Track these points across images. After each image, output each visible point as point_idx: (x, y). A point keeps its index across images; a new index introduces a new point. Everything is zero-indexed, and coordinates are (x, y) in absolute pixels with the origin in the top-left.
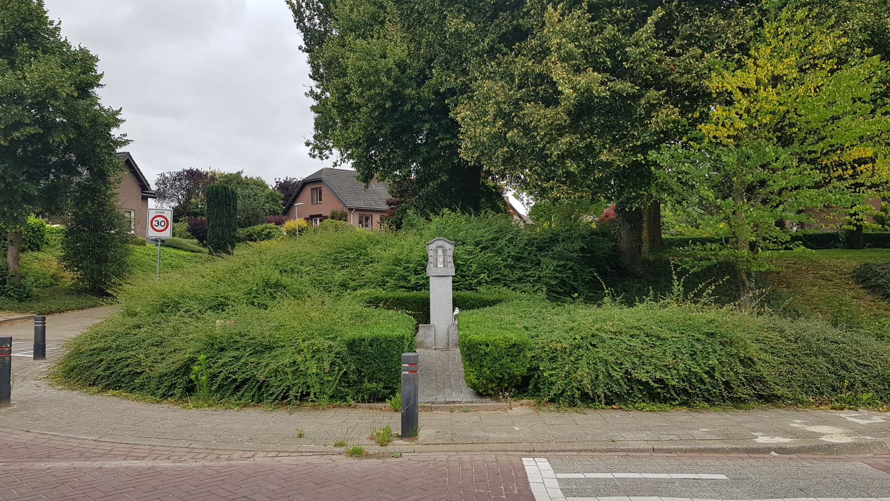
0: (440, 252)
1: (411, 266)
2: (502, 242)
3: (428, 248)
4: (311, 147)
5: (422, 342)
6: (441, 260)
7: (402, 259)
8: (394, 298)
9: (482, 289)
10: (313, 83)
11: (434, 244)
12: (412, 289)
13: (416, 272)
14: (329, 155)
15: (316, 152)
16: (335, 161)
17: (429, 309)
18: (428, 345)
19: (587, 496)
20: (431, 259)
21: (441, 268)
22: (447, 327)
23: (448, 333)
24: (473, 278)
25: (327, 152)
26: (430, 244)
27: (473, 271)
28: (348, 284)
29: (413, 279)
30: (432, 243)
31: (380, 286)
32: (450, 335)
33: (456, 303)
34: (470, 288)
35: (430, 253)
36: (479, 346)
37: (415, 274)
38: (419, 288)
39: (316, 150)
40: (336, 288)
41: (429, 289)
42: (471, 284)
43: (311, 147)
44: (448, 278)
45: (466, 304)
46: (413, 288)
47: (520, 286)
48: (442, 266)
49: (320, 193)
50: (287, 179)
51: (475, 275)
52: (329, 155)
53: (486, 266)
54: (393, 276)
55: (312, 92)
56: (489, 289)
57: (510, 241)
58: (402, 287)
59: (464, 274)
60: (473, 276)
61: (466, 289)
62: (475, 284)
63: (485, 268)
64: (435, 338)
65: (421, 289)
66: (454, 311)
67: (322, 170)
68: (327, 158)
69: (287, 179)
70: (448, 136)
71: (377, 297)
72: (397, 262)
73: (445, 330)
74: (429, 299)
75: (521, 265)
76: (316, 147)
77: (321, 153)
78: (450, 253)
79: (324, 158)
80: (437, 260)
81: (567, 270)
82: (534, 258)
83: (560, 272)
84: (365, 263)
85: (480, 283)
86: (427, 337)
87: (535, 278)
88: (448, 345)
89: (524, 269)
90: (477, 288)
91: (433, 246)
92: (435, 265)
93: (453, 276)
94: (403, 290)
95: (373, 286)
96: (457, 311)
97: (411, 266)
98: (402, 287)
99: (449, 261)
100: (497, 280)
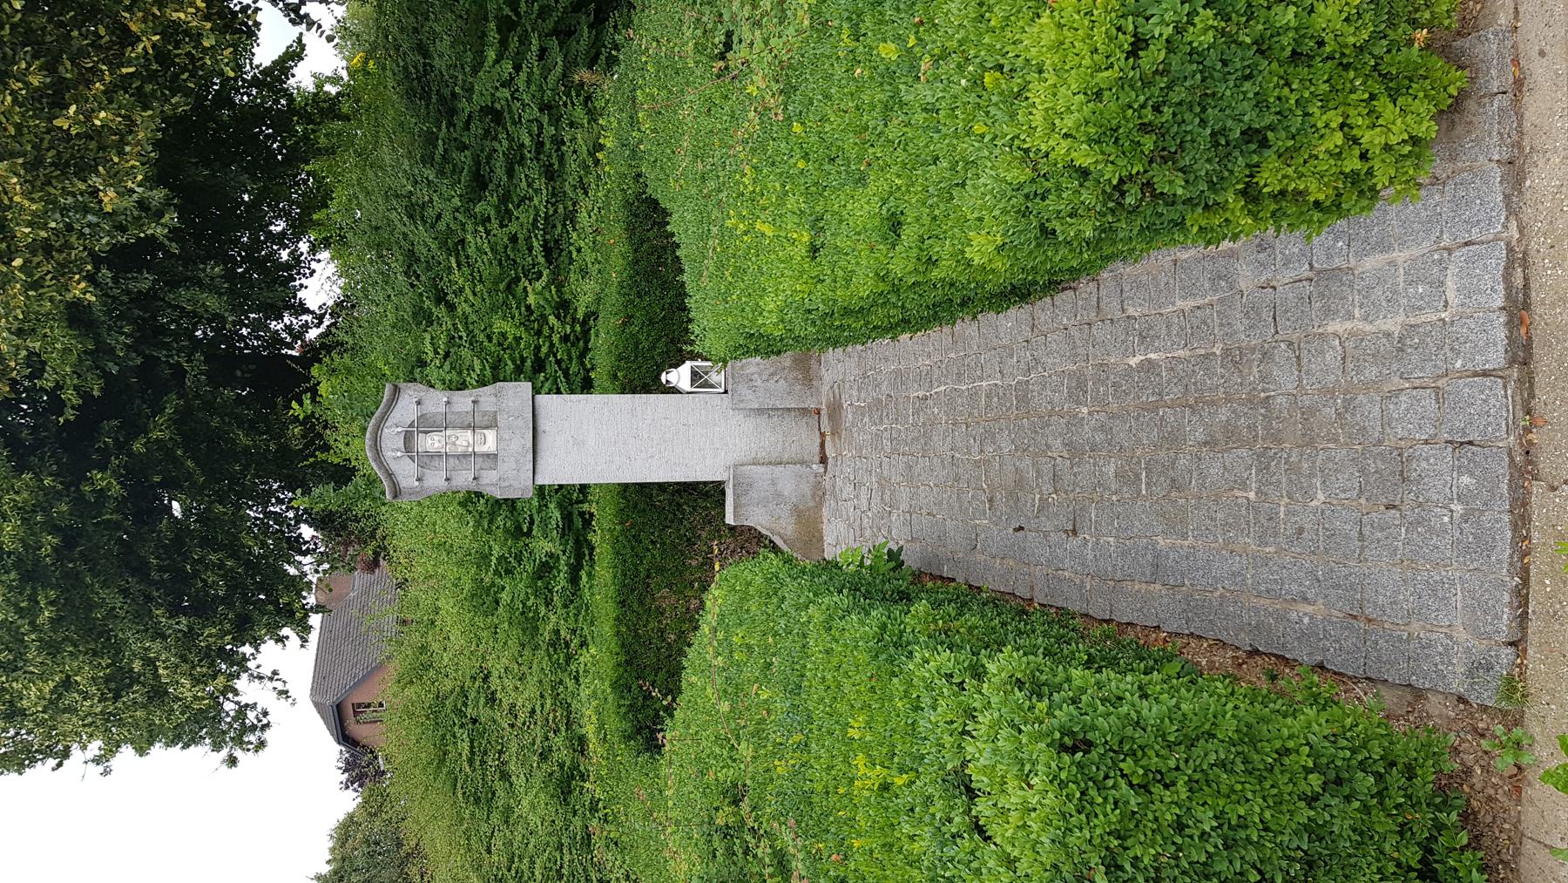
0: (432, 442)
1: (497, 551)
2: (423, 239)
3: (413, 492)
4: (238, 753)
5: (799, 513)
6: (464, 440)
7: (474, 580)
8: (617, 619)
9: (584, 294)
10: (77, 754)
11: (394, 467)
12: (581, 552)
13: (519, 533)
14: (259, 710)
15: (252, 738)
16: (275, 694)
17: (662, 487)
18: (806, 489)
20: (464, 480)
21: (499, 439)
23: (760, 411)
24: (546, 331)
25: (251, 715)
27: (521, 332)
28: (561, 766)
29: (544, 546)
30: (390, 475)
31: (569, 658)
32: (770, 403)
33: (649, 383)
34: (581, 339)
35: (436, 481)
36: (1153, 56)
37: (529, 534)
38: (578, 523)
39: (246, 739)
40: (577, 822)
41: (584, 488)
42: (565, 339)
43: (238, 753)
44: (541, 412)
45: (646, 344)
46: (577, 542)
47: (572, 165)
48: (491, 435)
49: (359, 705)
50: (340, 768)
51: (533, 321)
53: (502, 286)
54: (536, 612)
55: (97, 761)
56: (584, 273)
57: (415, 211)
58: (574, 579)
59: (528, 363)
60: (539, 333)
61: (582, 355)
62: (564, 323)
63: (508, 287)
64: (770, 463)
65: (582, 514)
66: (674, 391)
67: (316, 704)
68: (265, 714)
69: (340, 768)
71: (614, 686)
72: (484, 599)
73: (749, 424)
74: (625, 487)
75: (500, 172)
76: (239, 741)
77: (253, 728)
78: (436, 400)
79: (265, 721)
80: (465, 456)
81: (518, 14)
82: (476, 128)
83: (524, 41)
84: (492, 700)
85: (563, 307)
86: (779, 495)
87: (545, 120)
88: (804, 412)
89: (515, 160)
90: (580, 315)
91: (406, 473)
92: (489, 463)
93: (536, 391)
94: (585, 578)
95: (570, 683)
96: (680, 376)
97: (497, 551)
98: (574, 579)
99: (470, 407)
100: (551, 250)
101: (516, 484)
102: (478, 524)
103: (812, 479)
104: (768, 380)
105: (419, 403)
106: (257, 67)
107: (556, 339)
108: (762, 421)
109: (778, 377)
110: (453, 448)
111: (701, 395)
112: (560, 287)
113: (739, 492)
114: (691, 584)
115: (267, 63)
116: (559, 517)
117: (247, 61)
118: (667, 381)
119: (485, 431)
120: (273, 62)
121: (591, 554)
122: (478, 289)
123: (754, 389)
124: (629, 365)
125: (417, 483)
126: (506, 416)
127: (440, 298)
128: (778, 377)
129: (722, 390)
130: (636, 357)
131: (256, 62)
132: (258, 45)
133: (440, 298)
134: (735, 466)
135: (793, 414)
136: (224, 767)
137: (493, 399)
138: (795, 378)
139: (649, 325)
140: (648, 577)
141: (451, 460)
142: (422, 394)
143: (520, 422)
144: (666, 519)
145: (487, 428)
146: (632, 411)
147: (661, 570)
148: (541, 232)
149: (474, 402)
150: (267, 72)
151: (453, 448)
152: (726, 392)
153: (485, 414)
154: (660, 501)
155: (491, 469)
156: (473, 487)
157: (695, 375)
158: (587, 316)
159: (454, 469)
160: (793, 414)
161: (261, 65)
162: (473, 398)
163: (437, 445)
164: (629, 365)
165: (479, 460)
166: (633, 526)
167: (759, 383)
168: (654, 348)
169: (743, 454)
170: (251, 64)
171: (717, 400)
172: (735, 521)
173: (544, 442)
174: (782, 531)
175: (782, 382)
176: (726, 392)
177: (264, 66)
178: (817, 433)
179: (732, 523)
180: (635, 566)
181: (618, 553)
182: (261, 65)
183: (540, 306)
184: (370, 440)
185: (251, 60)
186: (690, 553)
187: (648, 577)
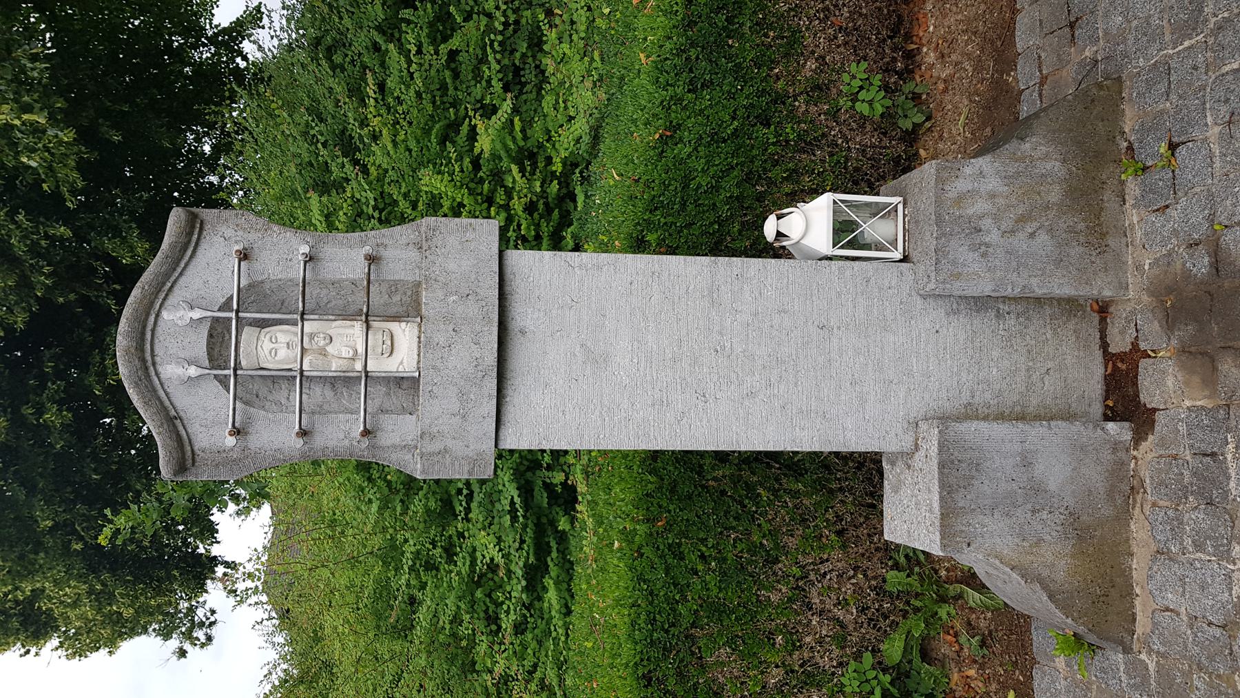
3: (223, 458)
4: (187, 646)
11: (183, 401)
15: (200, 634)
17: (722, 457)
18: (1095, 476)
19: (703, 255)
21: (423, 344)
22: (935, 314)
23: (980, 304)
25: (200, 613)
26: (181, 443)
39: (195, 635)
42: (530, 208)
45: (704, 181)
48: (405, 334)
52: (207, 607)
64: (1022, 418)
68: (213, 612)
70: (98, 359)
77: (202, 624)
79: (212, 619)
85: (529, 158)
86: (1036, 489)
92: (400, 398)
101: (457, 447)
102: (385, 505)
103: (1107, 455)
104: (1013, 232)
105: (244, 256)
106: (217, 26)
107: (517, 205)
108: (984, 323)
109: (1035, 224)
110: (320, 362)
111: (875, 263)
112: (527, 125)
113: (952, 480)
114: (770, 635)
115: (225, 24)
116: (515, 493)
117: (208, 21)
118: (779, 235)
119: (394, 326)
120: (231, 23)
121: (564, 552)
122: (401, 137)
123: (983, 248)
124: (670, 219)
125: (231, 441)
126: (440, 294)
127: (348, 147)
128: (1035, 224)
129: (898, 255)
130: (683, 205)
131: (215, 22)
132: (218, 6)
133: (348, 147)
134: (944, 419)
135: (1048, 311)
136: (175, 658)
137: (413, 254)
138: (1071, 230)
139: (709, 144)
140: (693, 625)
141: (317, 390)
142: (253, 236)
143: (471, 309)
144: (727, 513)
145: (396, 318)
146: (711, 292)
147: (718, 611)
148: (500, 38)
149: (372, 259)
150: (225, 31)
151: (320, 362)
152: (905, 259)
153: (394, 287)
154: (715, 479)
155: (404, 411)
156: (362, 449)
157: (843, 230)
158: (571, 164)
159: (321, 410)
160: (1048, 311)
161: (220, 25)
162: (367, 249)
163: (283, 353)
164: (670, 219)
165: (378, 391)
166: (669, 527)
167: (994, 237)
168: (715, 189)
169: (944, 394)
170: (211, 24)
171: (890, 275)
172: (944, 547)
173: (522, 356)
174: (1045, 573)
175: (1043, 237)
176: (905, 259)
177: (222, 26)
178: (1098, 354)
179: (928, 540)
180: (673, 603)
181: (641, 579)
182: (220, 25)
183: (495, 157)
184: (128, 334)
185: (211, 20)
186: (767, 577)
187: (693, 625)
